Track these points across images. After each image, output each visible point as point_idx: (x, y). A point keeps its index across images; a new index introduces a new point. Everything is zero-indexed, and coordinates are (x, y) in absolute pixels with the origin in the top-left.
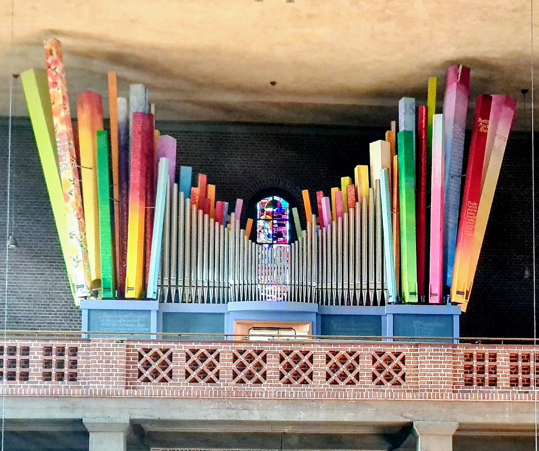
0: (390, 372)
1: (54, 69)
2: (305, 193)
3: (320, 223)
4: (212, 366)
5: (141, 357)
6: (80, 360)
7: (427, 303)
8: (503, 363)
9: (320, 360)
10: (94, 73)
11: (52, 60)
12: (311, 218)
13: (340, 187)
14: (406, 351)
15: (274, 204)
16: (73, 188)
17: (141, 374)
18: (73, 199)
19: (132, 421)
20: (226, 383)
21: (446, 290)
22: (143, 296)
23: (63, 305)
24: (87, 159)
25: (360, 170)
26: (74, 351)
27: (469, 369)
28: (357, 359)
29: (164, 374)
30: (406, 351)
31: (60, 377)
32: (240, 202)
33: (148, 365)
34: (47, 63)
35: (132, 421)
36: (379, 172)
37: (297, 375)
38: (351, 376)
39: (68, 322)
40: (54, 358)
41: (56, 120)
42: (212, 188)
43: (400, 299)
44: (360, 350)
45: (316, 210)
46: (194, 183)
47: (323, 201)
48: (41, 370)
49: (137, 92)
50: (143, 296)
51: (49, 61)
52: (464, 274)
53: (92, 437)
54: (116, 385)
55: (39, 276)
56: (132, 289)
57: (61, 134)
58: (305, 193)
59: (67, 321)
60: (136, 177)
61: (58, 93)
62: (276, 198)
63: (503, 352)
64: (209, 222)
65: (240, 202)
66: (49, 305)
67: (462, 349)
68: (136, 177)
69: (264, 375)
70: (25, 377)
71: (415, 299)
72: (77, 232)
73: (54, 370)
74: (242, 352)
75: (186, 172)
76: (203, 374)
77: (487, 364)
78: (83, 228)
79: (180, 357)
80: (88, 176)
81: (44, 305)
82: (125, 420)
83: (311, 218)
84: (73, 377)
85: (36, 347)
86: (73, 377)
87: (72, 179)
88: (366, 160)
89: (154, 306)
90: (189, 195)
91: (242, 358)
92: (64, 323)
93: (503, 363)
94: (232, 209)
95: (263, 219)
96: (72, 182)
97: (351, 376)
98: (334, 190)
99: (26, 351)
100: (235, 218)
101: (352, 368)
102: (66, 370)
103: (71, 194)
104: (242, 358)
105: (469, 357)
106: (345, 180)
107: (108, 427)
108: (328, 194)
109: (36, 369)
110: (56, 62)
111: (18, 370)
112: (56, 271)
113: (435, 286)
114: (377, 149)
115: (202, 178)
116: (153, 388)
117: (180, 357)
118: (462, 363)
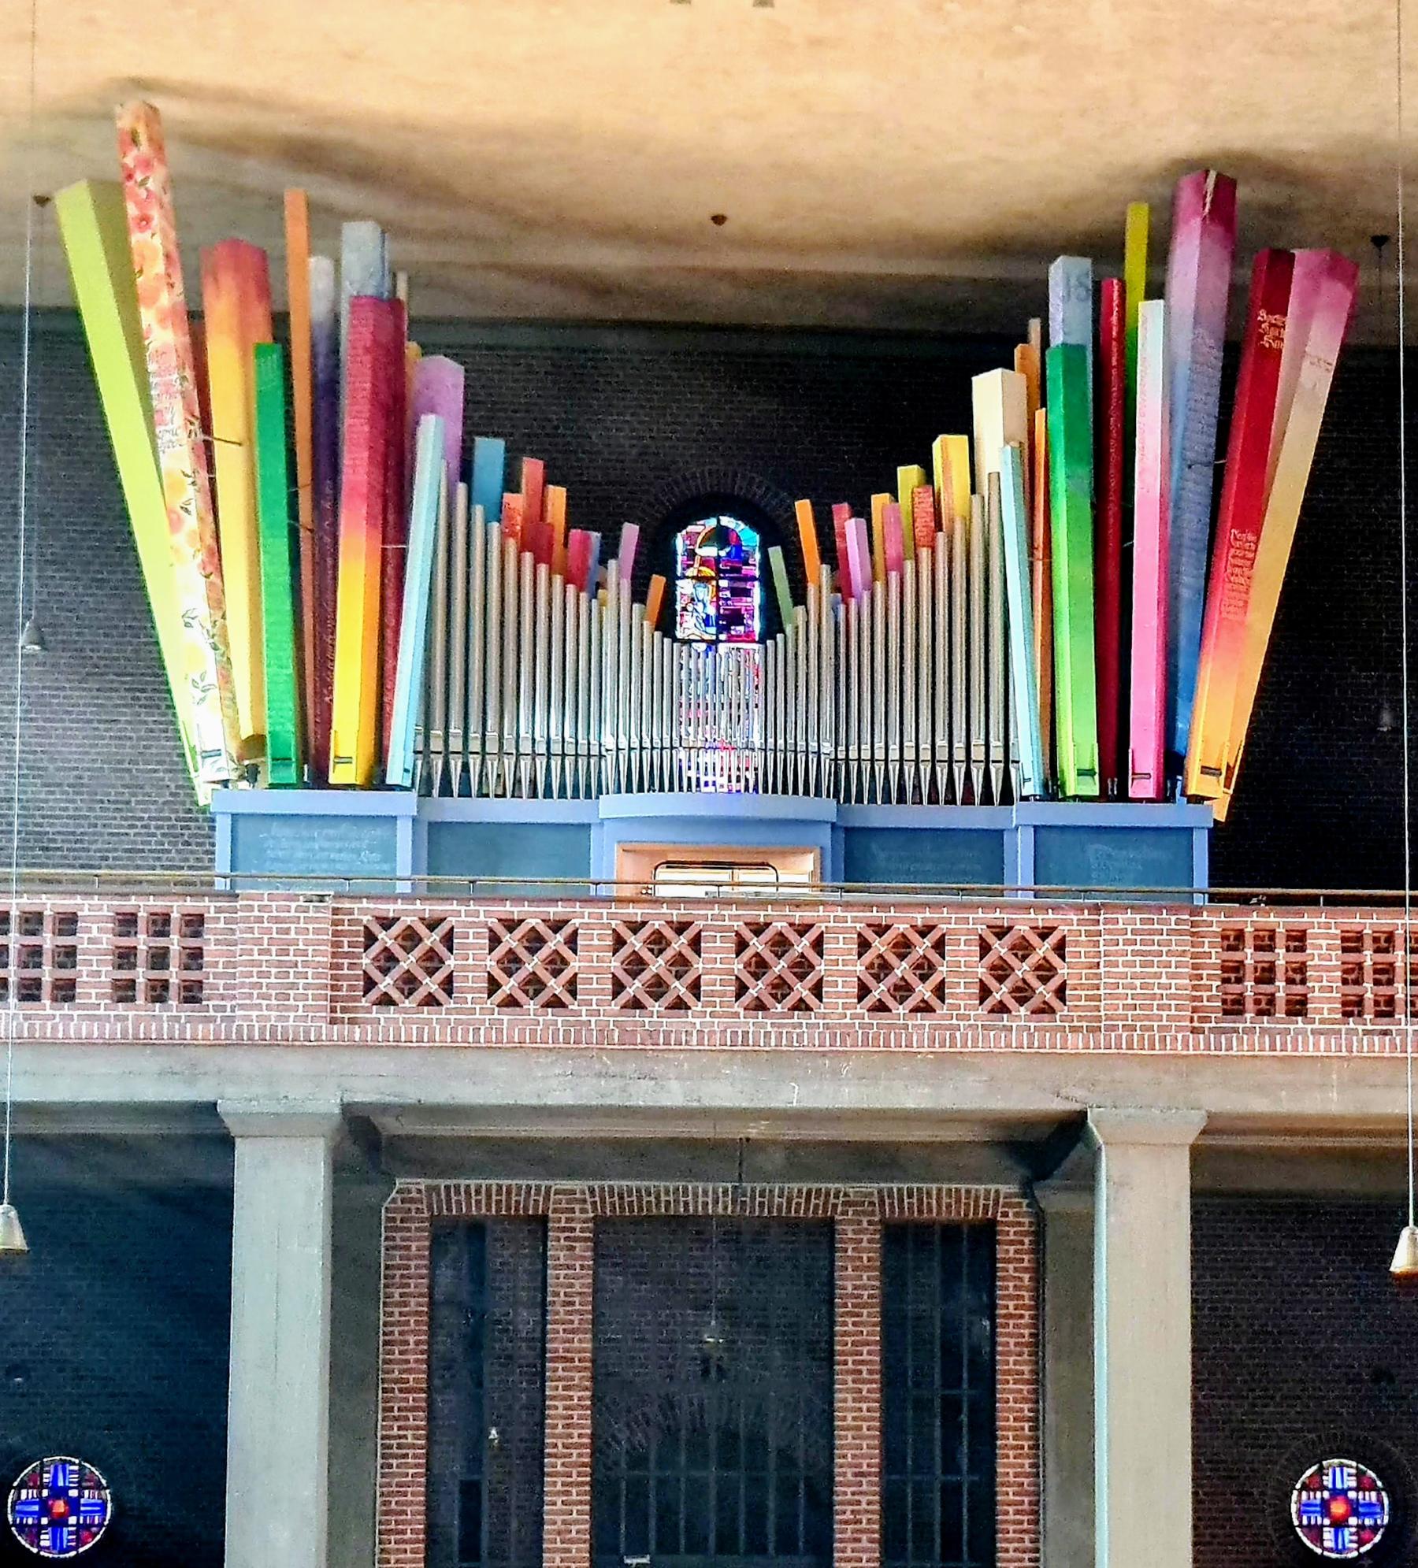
0: (1025, 980)
1: (143, 183)
2: (803, 509)
3: (842, 587)
4: (557, 964)
5: (371, 938)
6: (211, 948)
7: (1123, 797)
8: (1324, 955)
9: (841, 946)
10: (247, 191)
11: (136, 158)
12: (818, 574)
13: (894, 492)
14: (1069, 923)
15: (721, 536)
16: (192, 495)
17: (370, 984)
18: (191, 523)
19: (347, 1108)
20: (595, 1008)
21: (1173, 763)
22: (376, 780)
23: (164, 803)
24: (228, 418)
25: (947, 449)
26: (195, 924)
27: (1233, 972)
28: (939, 946)
29: (431, 985)
30: (1069, 923)
31: (159, 992)
32: (630, 533)
33: (388, 960)
34: (124, 166)
35: (347, 1108)
36: (996, 452)
37: (781, 988)
38: (924, 991)
39: (180, 847)
40: (142, 942)
41: (148, 317)
42: (557, 496)
43: (1053, 788)
44: (947, 921)
45: (831, 553)
46: (511, 483)
47: (851, 529)
48: (108, 973)
49: (361, 243)
50: (376, 780)
51: (129, 161)
52: (1220, 722)
53: (243, 1151)
54: (305, 1014)
55: (102, 726)
56: (348, 760)
57: (161, 353)
58: (803, 509)
59: (175, 844)
60: (357, 466)
61: (152, 245)
62: (726, 521)
63: (1324, 928)
64: (549, 585)
65: (630, 533)
66: (128, 802)
67: (1216, 920)
68: (357, 466)
69: (695, 988)
70: (66, 991)
71: (1092, 788)
72: (203, 611)
73: (141, 975)
74: (635, 927)
75: (490, 451)
76: (534, 985)
77: (1281, 957)
78: (217, 601)
79: (473, 941)
80: (231, 464)
81: (117, 802)
82: (330, 1104)
83: (818, 574)
84: (192, 994)
85: (96, 914)
86: (192, 994)
87: (189, 473)
88: (962, 422)
89: (406, 804)
90: (497, 512)
91: (636, 943)
92: (169, 851)
93: (1324, 955)
94: (610, 550)
95: (693, 578)
96: (191, 480)
97: (924, 991)
98: (879, 501)
99: (68, 923)
100: (617, 575)
101: (925, 969)
102: (174, 975)
103: (187, 510)
104: (636, 943)
105: (1234, 940)
106: (908, 475)
107: (284, 1125)
108: (862, 510)
109: (95, 972)
110: (146, 165)
111: (47, 974)
112: (147, 714)
113: (1144, 752)
114: (992, 394)
115: (531, 469)
116: (403, 1021)
117: (473, 941)
118: (1216, 956)
